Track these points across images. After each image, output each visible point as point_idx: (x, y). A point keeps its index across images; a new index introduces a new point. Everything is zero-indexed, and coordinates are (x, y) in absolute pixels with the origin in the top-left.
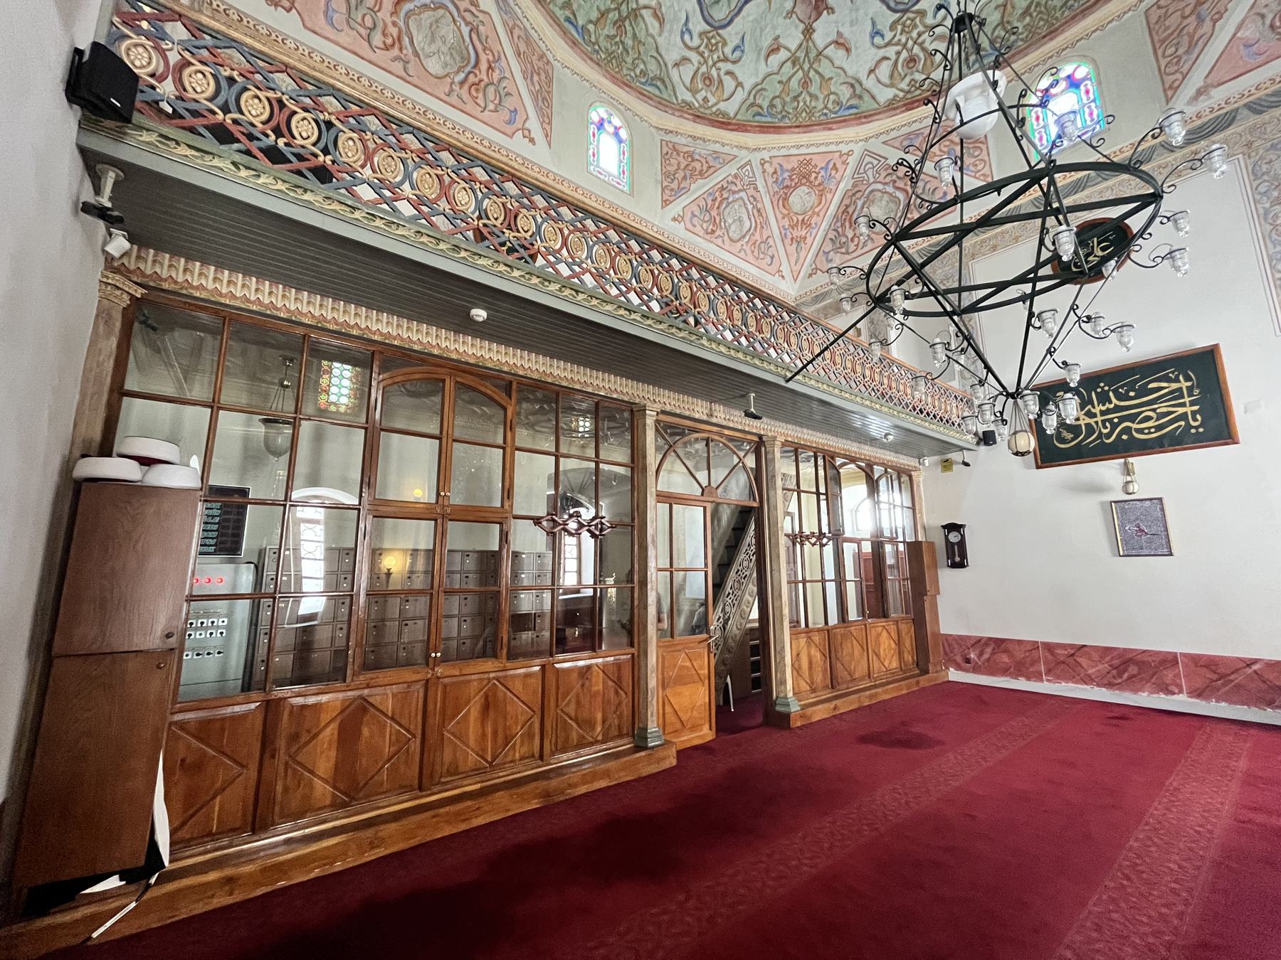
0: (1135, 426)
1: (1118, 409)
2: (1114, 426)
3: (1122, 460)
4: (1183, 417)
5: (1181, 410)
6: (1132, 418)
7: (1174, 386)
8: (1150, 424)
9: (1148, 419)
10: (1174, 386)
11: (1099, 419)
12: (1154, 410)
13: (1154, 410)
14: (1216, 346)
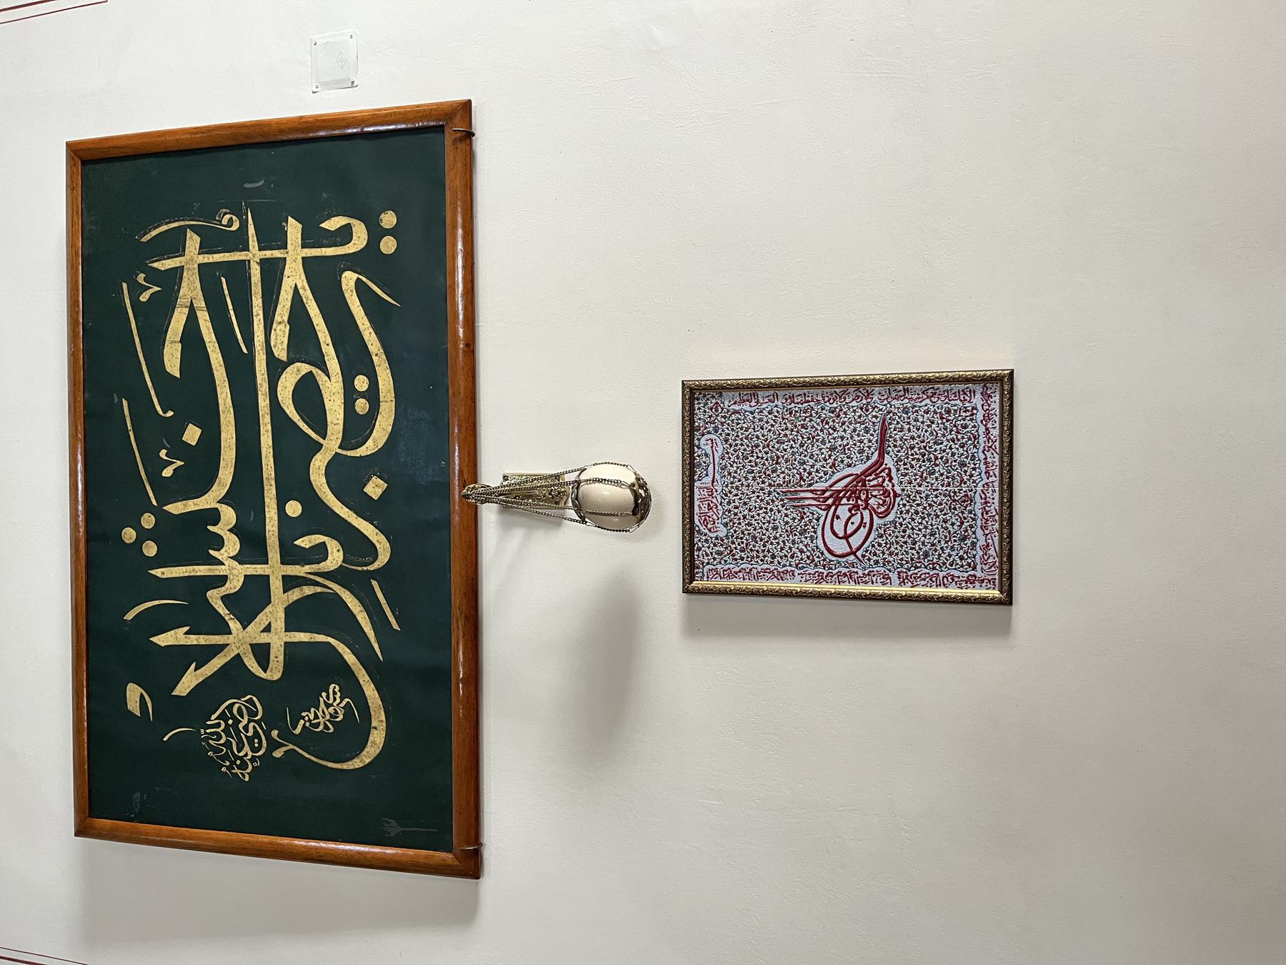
0: (332, 443)
1: (245, 493)
2: (318, 517)
3: (489, 515)
4: (322, 276)
5: (294, 277)
6: (293, 452)
7: (190, 289)
8: (332, 390)
9: (308, 394)
10: (190, 289)
11: (274, 569)
12: (276, 366)
13: (276, 366)
14: (68, 145)
